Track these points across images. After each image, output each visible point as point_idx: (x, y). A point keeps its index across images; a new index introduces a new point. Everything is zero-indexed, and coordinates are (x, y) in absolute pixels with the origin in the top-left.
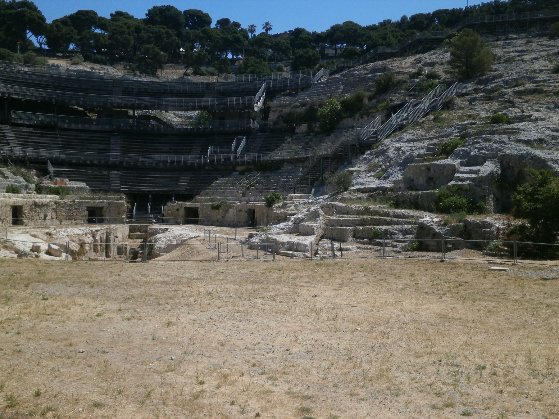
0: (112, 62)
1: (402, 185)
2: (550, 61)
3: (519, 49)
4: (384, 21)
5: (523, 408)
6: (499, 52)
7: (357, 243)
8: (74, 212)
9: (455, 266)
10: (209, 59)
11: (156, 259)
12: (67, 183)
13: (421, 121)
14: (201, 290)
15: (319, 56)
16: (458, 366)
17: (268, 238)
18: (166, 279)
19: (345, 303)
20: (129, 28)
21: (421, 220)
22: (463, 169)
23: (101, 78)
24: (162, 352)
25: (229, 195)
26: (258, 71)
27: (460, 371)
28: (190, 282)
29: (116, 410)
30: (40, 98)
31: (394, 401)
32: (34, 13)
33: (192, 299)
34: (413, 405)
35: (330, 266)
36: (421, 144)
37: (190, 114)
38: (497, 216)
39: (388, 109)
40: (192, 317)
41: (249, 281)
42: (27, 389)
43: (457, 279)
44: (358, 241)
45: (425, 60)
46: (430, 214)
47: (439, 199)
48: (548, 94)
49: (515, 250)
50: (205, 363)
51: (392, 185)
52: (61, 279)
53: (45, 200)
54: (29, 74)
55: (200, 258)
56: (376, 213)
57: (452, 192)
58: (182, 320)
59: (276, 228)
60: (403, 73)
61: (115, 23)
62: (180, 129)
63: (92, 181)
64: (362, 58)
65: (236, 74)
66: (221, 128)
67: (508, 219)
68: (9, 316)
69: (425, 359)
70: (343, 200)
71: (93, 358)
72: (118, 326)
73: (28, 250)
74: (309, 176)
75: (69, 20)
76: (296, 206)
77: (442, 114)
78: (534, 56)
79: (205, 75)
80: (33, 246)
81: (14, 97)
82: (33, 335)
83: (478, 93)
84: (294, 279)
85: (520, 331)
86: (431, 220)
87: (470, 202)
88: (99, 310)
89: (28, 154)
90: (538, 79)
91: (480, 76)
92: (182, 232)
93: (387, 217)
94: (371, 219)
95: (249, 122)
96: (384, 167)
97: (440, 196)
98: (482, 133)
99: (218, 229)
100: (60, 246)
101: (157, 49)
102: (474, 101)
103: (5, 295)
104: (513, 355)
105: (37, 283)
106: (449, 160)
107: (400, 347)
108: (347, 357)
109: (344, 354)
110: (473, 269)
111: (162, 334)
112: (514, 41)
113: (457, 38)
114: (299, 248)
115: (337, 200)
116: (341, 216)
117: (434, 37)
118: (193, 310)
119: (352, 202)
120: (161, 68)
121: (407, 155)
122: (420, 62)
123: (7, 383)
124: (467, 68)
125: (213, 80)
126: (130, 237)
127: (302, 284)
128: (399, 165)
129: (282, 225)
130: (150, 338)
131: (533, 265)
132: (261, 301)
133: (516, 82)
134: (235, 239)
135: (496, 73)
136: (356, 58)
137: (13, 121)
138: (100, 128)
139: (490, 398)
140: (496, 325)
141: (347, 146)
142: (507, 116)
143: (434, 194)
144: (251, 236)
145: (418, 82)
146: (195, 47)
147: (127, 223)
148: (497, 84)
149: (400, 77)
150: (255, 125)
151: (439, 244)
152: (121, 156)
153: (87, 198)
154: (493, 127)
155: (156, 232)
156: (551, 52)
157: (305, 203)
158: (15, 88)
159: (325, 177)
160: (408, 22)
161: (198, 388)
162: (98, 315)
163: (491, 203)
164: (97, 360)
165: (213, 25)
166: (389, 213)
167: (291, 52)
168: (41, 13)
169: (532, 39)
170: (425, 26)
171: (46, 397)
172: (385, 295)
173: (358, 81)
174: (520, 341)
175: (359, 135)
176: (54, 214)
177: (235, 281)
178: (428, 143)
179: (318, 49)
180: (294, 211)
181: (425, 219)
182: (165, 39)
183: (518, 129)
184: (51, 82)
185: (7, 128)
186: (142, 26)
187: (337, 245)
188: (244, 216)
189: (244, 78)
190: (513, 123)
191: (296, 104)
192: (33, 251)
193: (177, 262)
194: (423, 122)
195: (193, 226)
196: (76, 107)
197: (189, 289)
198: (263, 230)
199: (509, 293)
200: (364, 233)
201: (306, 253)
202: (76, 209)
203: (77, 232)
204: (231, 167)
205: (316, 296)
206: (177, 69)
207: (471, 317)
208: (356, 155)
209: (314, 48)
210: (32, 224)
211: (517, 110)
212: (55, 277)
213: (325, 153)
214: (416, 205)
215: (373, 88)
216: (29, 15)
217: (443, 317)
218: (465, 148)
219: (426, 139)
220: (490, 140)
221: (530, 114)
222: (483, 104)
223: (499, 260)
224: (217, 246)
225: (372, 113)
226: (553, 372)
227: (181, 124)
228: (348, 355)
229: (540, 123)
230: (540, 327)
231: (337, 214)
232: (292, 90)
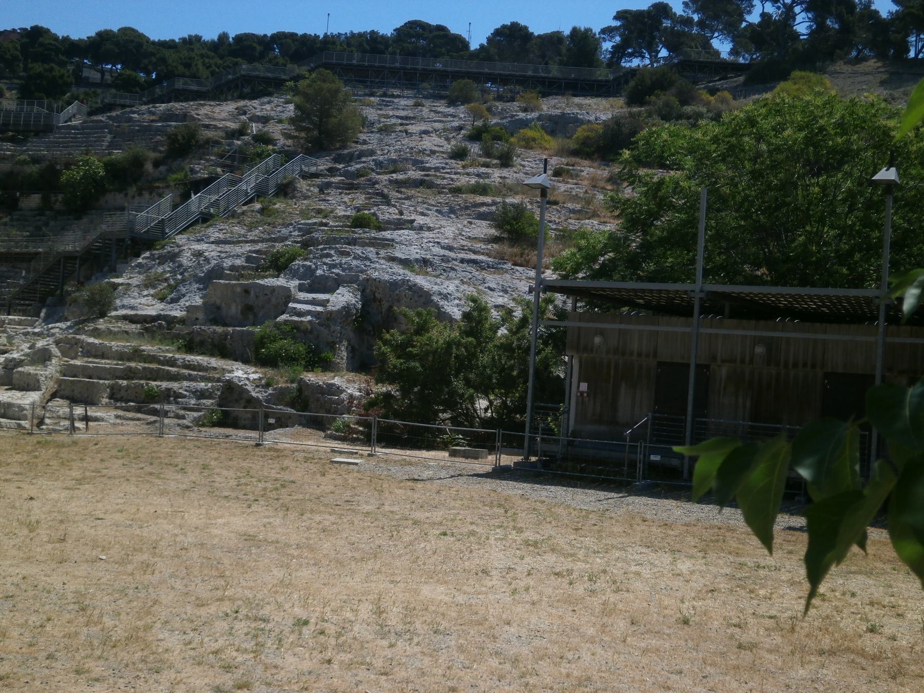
1: (201, 315)
2: (448, 140)
3: (402, 113)
4: (190, 36)
5: (360, 688)
6: (371, 114)
7: (117, 408)
9: (278, 453)
13: (239, 211)
15: (72, 79)
16: (264, 621)
19: (84, 512)
21: (228, 376)
22: (302, 296)
27: (267, 628)
31: (151, 681)
34: (183, 687)
35: (63, 446)
36: (238, 250)
38: (351, 376)
39: (185, 184)
43: (279, 476)
44: (118, 404)
45: (254, 111)
46: (244, 367)
47: (261, 342)
48: (440, 189)
49: (374, 432)
51: (184, 313)
56: (152, 359)
57: (283, 333)
60: (216, 127)
64: (147, 93)
67: (367, 382)
69: (213, 609)
70: (96, 333)
74: (39, 286)
76: (10, 338)
77: (275, 204)
78: (423, 128)
83: (335, 176)
85: (369, 562)
86: (245, 376)
87: (310, 351)
90: (427, 165)
91: (340, 149)
93: (172, 366)
94: (144, 368)
96: (172, 282)
97: (262, 338)
98: (335, 241)
102: (327, 188)
104: (353, 602)
106: (280, 279)
107: (173, 588)
108: (76, 607)
109: (73, 600)
110: (306, 460)
112: (396, 100)
113: (307, 82)
114: (10, 413)
115: (85, 333)
116: (90, 360)
117: (270, 75)
119: (112, 336)
121: (212, 265)
122: (245, 113)
124: (320, 134)
127: (8, 477)
128: (199, 280)
131: (400, 458)
133: (394, 166)
135: (365, 147)
136: (137, 92)
139: (310, 673)
140: (333, 553)
141: (110, 240)
142: (377, 219)
143: (252, 333)
145: (240, 146)
148: (365, 165)
149: (210, 134)
151: (255, 416)
154: (354, 232)
156: (449, 126)
157: (26, 334)
159: (67, 291)
160: (230, 44)
163: (343, 353)
166: (176, 360)
167: (21, 65)
169: (424, 101)
170: (257, 54)
172: (156, 500)
173: (138, 131)
174: (367, 579)
175: (132, 222)
178: (248, 249)
179: (71, 68)
180: (5, 345)
181: (236, 374)
183: (393, 240)
187: (79, 411)
190: (385, 230)
191: (22, 157)
194: (243, 213)
199: (359, 501)
200: (129, 392)
201: (22, 422)
205: (31, 499)
207: (294, 538)
208: (125, 258)
209: (63, 64)
211: (392, 210)
213: (70, 248)
214: (222, 350)
215: (163, 146)
217: (249, 538)
218: (308, 263)
219: (247, 242)
220: (348, 254)
221: (413, 218)
222: (341, 193)
223: (349, 447)
225: (158, 188)
226: (412, 629)
228: (78, 602)
229: (426, 234)
230: (400, 556)
231: (83, 356)
232: (18, 132)
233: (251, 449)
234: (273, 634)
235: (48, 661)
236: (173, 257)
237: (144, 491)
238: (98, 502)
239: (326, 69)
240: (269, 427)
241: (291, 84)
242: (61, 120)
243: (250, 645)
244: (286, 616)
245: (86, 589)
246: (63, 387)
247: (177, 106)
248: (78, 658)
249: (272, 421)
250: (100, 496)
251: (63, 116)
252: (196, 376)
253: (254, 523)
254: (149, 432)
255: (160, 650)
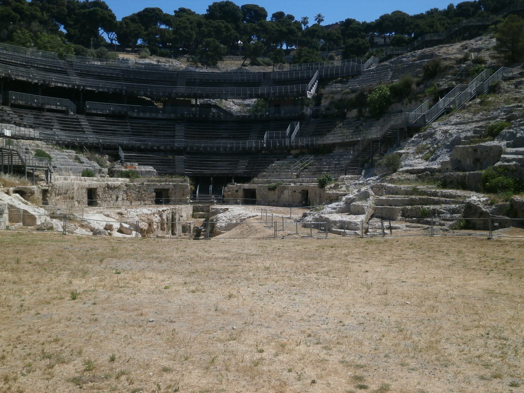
0: (176, 55)
1: (450, 167)
4: (431, 10)
7: (406, 221)
8: (143, 194)
9: (502, 243)
10: (265, 50)
11: (217, 237)
12: (137, 167)
13: (467, 105)
14: (259, 265)
16: (505, 339)
17: (321, 217)
18: (227, 255)
19: (395, 278)
20: (191, 23)
21: (468, 200)
22: (509, 150)
23: (167, 70)
24: (224, 322)
25: (284, 177)
26: (311, 60)
27: (507, 344)
28: (249, 257)
29: (183, 375)
30: (111, 90)
31: (443, 371)
32: (105, 12)
33: (251, 274)
34: (462, 375)
35: (380, 243)
36: (468, 127)
37: (248, 102)
39: (435, 94)
40: (252, 290)
41: (303, 257)
42: (103, 355)
43: (504, 256)
45: (472, 46)
46: (476, 194)
47: (486, 179)
50: (264, 332)
52: (132, 255)
53: (116, 183)
54: (102, 68)
55: (258, 235)
56: (424, 193)
58: (242, 292)
59: (328, 208)
60: (450, 59)
61: (179, 19)
62: (239, 116)
63: (159, 165)
64: (410, 45)
65: (290, 63)
66: (277, 115)
68: (86, 288)
69: (474, 332)
70: (392, 181)
71: (162, 327)
72: (185, 298)
73: (102, 228)
75: (137, 18)
76: (347, 187)
77: (488, 98)
79: (262, 65)
80: (106, 225)
81: (88, 89)
82: (107, 305)
84: (346, 255)
86: (478, 199)
88: (167, 283)
89: (101, 141)
92: (241, 212)
93: (435, 196)
94: (420, 199)
95: (302, 109)
97: (487, 176)
99: (274, 208)
100: (131, 225)
101: (217, 43)
103: (82, 269)
105: (111, 259)
106: (495, 141)
107: (449, 320)
108: (397, 329)
109: (395, 326)
111: (224, 305)
113: (503, 24)
114: (350, 227)
115: (386, 181)
117: (480, 23)
118: (252, 284)
119: (401, 182)
120: (221, 59)
121: (454, 137)
122: (466, 48)
123: (85, 349)
125: (269, 69)
126: (193, 216)
127: (354, 260)
128: (447, 147)
129: (334, 205)
130: (213, 309)
132: (315, 275)
134: (290, 218)
136: (404, 46)
137: (87, 111)
138: (166, 116)
143: (481, 174)
144: (305, 215)
145: (465, 68)
146: (252, 40)
147: (191, 203)
149: (447, 63)
150: (308, 111)
151: (485, 222)
152: (185, 142)
153: (155, 181)
155: (217, 212)
157: (355, 184)
158: (89, 81)
159: (375, 160)
160: (455, 10)
161: (258, 356)
162: (166, 288)
164: (166, 328)
165: (268, 19)
166: (437, 193)
167: (342, 41)
168: (111, 11)
171: (120, 362)
175: (407, 119)
176: (125, 195)
177: (290, 257)
178: (474, 126)
179: (368, 38)
180: (345, 191)
181: (472, 198)
182: (224, 33)
184: (121, 75)
185: (82, 117)
186: (203, 21)
187: (386, 224)
188: (298, 196)
189: (298, 68)
191: (346, 90)
192: (107, 230)
193: (236, 240)
194: (470, 106)
195: (251, 206)
196: (144, 97)
197: (248, 264)
198: (316, 210)
200: (412, 212)
201: (357, 232)
202: (144, 191)
203: (145, 212)
204: (286, 151)
205: (367, 271)
206: (235, 60)
208: (405, 138)
209: (363, 37)
210: (105, 205)
212: (127, 253)
213: (374, 136)
214: (463, 185)
215: (421, 73)
216: (101, 13)
217: (491, 292)
218: (511, 130)
219: (473, 122)
224: (274, 225)
225: (420, 97)
227: (240, 112)
231: (386, 194)
233: (485, 241)
234: (512, 348)
235: (385, 359)
236: (431, 135)
237: (426, 266)
238: (402, 272)
239: (514, 14)
240: (495, 228)
241: (493, 26)
242: (365, 67)
243: (498, 353)
244: (518, 337)
245: (401, 320)
246: (376, 211)
247: (427, 50)
248: (401, 357)
249: (496, 224)
250: (402, 270)
251: (366, 65)
252: (449, 201)
253: (492, 283)
254: (425, 234)
255: (446, 354)
